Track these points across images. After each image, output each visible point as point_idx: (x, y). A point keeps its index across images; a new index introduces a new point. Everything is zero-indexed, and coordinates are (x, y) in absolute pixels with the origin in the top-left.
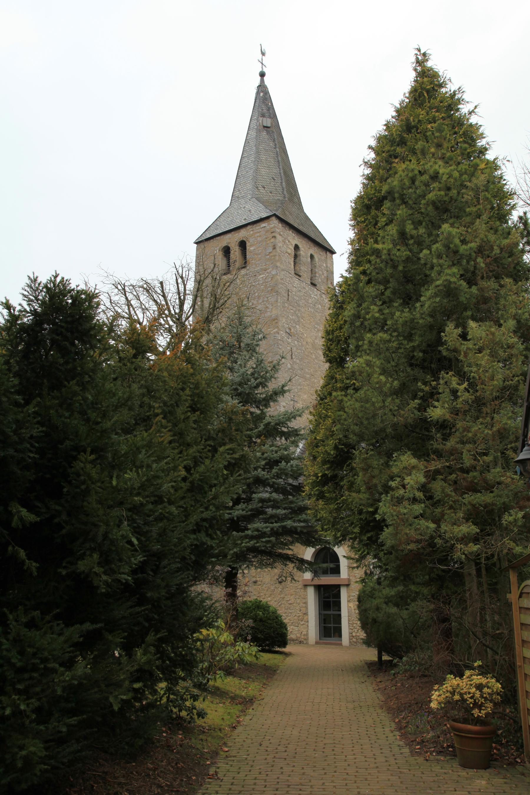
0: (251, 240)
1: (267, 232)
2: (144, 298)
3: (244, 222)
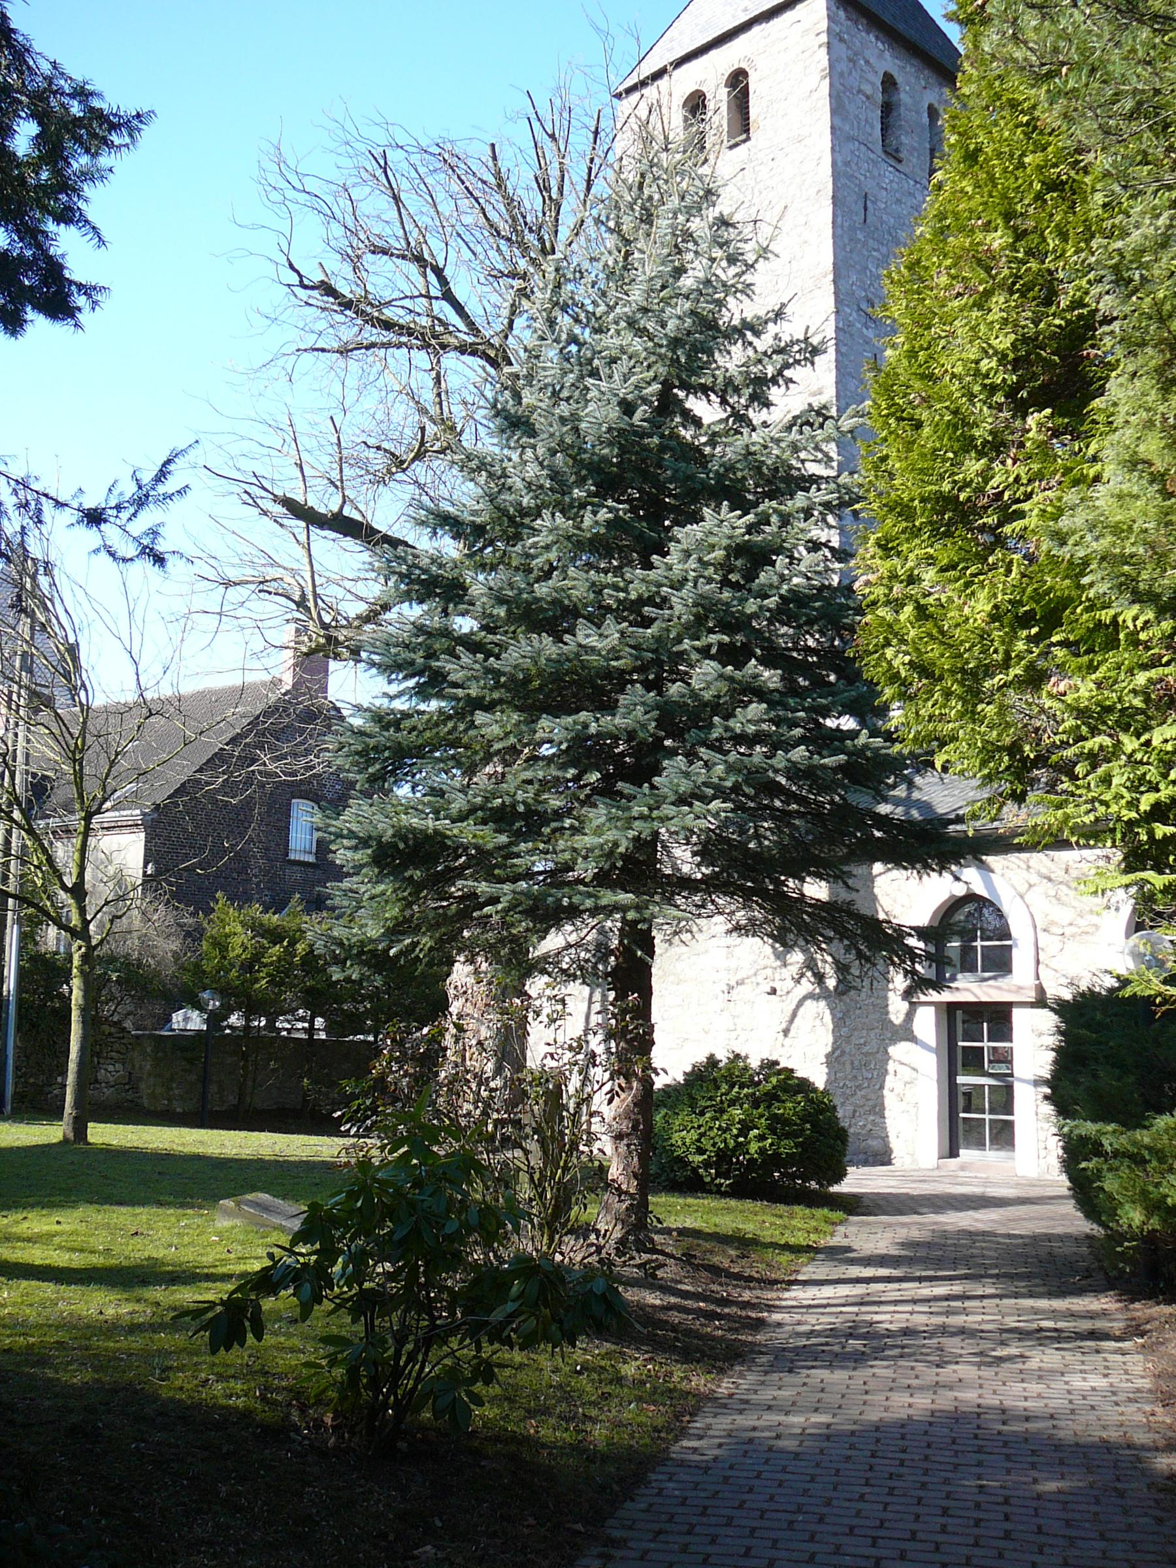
2: (439, 181)
3: (744, 18)
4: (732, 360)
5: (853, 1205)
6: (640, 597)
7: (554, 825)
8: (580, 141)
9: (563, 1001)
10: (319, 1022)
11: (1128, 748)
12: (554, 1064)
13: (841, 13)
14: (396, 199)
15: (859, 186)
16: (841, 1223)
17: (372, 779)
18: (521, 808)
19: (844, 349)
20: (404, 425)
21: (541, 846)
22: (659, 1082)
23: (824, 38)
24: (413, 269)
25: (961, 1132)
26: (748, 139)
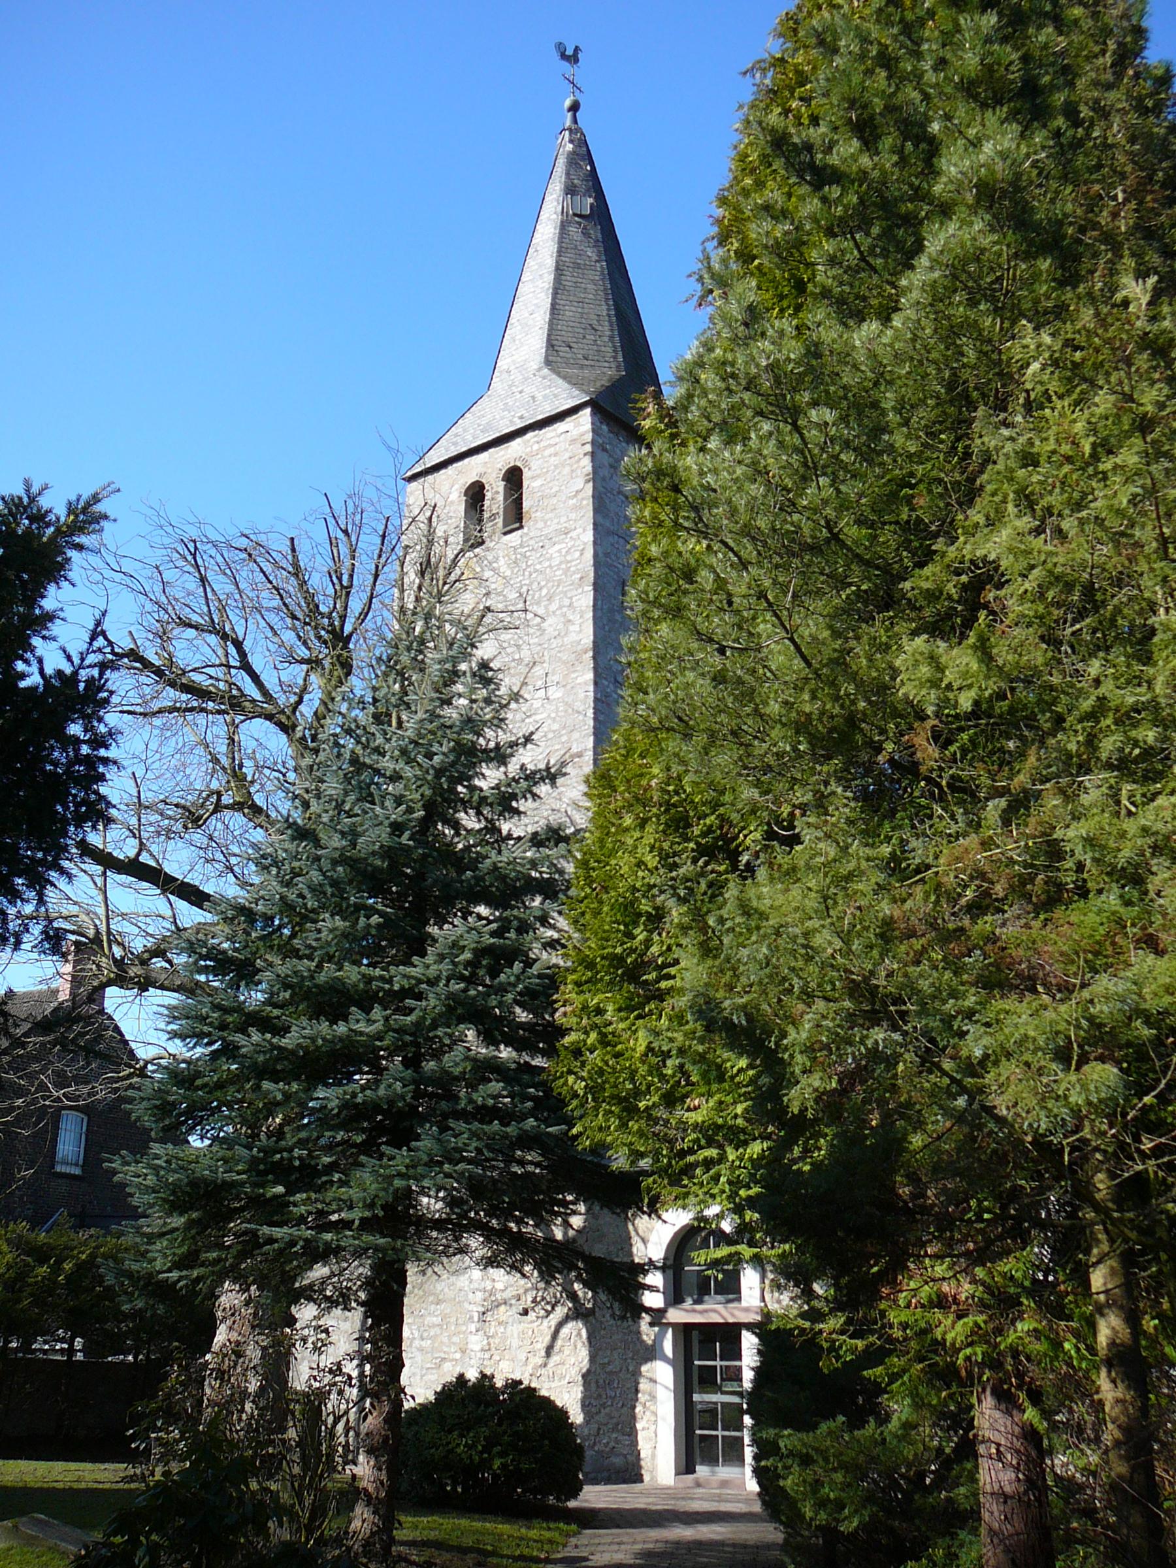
0: (535, 464)
1: (573, 441)
2: (247, 574)
4: (489, 778)
5: (591, 1519)
6: (402, 988)
7: (324, 1179)
8: (369, 543)
9: (326, 1331)
10: (78, 1343)
11: (731, 1158)
12: (317, 1385)
13: (604, 427)
14: (203, 580)
15: (618, 574)
16: (575, 1535)
17: (166, 1129)
18: (297, 1163)
19: (601, 718)
20: (199, 778)
21: (313, 1196)
22: (408, 1405)
23: (588, 448)
24: (213, 639)
25: (697, 1452)
26: (521, 527)
